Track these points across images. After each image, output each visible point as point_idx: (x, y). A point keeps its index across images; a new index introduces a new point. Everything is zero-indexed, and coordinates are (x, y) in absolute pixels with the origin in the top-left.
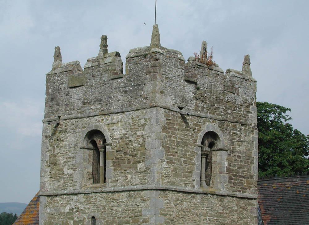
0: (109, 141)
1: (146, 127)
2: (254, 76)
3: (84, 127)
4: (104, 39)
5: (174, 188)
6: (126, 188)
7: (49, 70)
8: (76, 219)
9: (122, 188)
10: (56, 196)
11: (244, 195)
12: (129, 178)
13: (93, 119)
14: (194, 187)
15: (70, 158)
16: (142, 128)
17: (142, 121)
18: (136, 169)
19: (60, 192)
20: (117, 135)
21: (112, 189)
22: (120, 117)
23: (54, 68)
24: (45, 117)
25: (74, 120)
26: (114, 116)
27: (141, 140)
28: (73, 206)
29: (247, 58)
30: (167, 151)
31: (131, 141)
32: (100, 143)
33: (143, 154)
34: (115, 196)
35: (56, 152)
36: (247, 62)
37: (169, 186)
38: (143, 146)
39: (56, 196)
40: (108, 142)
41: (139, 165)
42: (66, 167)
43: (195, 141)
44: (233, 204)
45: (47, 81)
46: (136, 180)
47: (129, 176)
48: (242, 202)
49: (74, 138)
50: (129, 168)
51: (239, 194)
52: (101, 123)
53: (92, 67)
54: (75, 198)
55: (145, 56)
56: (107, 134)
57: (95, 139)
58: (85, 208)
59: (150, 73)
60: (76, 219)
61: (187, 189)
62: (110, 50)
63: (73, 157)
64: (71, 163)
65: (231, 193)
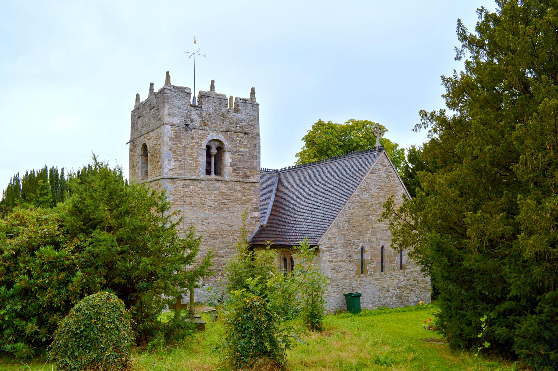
2: (258, 101)
5: (181, 177)
29: (253, 89)
36: (253, 92)
37: (176, 176)
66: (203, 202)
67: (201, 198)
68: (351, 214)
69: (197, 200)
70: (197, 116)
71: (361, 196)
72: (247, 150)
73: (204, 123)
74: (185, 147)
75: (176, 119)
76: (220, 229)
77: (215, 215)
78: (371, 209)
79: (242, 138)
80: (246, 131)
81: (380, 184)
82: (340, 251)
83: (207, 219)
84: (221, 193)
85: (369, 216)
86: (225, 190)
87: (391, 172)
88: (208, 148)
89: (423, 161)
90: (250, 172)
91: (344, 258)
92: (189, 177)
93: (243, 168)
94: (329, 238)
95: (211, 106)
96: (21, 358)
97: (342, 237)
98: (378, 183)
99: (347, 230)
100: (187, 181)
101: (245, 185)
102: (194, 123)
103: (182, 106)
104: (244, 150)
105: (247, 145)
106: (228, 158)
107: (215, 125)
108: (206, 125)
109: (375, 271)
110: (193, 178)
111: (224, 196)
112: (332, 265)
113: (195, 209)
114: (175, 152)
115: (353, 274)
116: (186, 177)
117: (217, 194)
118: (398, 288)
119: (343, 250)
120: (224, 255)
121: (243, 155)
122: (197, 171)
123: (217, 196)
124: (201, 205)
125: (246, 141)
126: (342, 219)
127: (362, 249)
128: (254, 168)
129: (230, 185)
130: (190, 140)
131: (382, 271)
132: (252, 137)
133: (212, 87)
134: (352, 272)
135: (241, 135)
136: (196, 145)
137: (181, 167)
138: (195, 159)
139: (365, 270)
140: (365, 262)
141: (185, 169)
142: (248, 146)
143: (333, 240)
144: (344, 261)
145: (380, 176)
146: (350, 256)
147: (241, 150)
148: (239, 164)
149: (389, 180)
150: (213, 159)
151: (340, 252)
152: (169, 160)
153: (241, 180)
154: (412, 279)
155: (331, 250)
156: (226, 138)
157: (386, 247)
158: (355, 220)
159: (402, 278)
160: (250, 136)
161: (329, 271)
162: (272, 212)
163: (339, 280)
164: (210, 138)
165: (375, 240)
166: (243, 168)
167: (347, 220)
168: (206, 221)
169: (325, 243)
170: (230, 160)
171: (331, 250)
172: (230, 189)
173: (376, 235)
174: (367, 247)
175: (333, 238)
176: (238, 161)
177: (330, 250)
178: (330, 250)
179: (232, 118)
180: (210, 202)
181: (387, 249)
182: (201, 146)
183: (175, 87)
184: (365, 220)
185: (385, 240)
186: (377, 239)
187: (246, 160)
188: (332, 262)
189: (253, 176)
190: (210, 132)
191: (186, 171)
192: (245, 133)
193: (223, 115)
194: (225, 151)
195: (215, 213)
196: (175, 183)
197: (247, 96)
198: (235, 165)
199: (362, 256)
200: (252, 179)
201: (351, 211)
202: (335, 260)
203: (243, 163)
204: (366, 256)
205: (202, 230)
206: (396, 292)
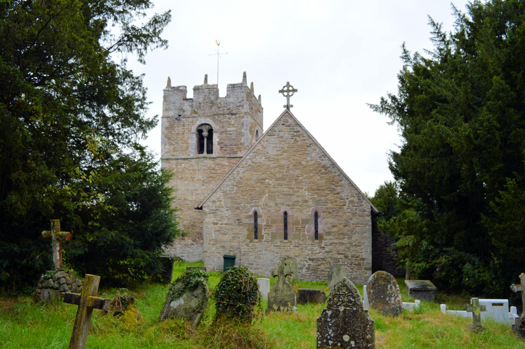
5: (174, 157)
29: (245, 74)
37: (171, 157)
66: (193, 176)
67: (191, 174)
68: (241, 178)
69: (187, 175)
70: (189, 107)
71: (253, 160)
72: (235, 129)
73: (195, 111)
74: (178, 134)
75: (171, 112)
77: (204, 187)
78: (268, 173)
79: (229, 119)
80: (234, 112)
81: (281, 146)
82: (227, 214)
83: (196, 190)
84: (209, 169)
85: (265, 179)
86: (213, 166)
87: (299, 132)
88: (200, 132)
90: (237, 148)
91: (231, 221)
92: (180, 157)
93: (230, 145)
94: (214, 202)
95: (201, 96)
97: (229, 200)
98: (278, 146)
99: (235, 193)
100: (180, 160)
101: (233, 161)
102: (185, 113)
103: (177, 101)
104: (232, 129)
105: (235, 124)
106: (216, 138)
107: (204, 112)
108: (196, 113)
109: (274, 236)
110: (183, 157)
111: (212, 171)
112: (217, 227)
113: (186, 182)
114: (169, 139)
115: (242, 238)
116: (178, 157)
117: (205, 170)
118: (312, 260)
119: (230, 213)
121: (231, 134)
122: (188, 152)
123: (206, 171)
124: (191, 179)
125: (233, 121)
126: (229, 183)
127: (256, 213)
128: (241, 144)
129: (217, 161)
130: (182, 127)
131: (286, 238)
132: (239, 117)
134: (241, 236)
135: (228, 116)
136: (187, 131)
137: (175, 150)
138: (186, 142)
139: (259, 235)
140: (259, 227)
141: (177, 151)
142: (236, 125)
143: (218, 204)
144: (231, 224)
145: (281, 137)
146: (238, 220)
147: (229, 129)
148: (226, 142)
149: (296, 140)
150: (205, 140)
151: (227, 215)
153: (228, 156)
154: (334, 252)
155: (216, 213)
156: (214, 121)
157: (290, 213)
158: (246, 184)
159: (317, 249)
160: (238, 115)
161: (213, 232)
163: (225, 242)
164: (198, 123)
165: (273, 205)
166: (230, 145)
167: (235, 183)
168: (195, 192)
169: (208, 206)
170: (218, 140)
171: (216, 213)
172: (217, 165)
173: (275, 200)
174: (260, 212)
175: (218, 201)
176: (225, 140)
177: (214, 212)
178: (214, 212)
179: (220, 103)
180: (199, 176)
181: (293, 216)
182: (191, 131)
183: (174, 87)
184: (259, 184)
185: (289, 205)
186: (276, 204)
187: (233, 137)
188: (217, 224)
189: (241, 151)
190: (199, 118)
191: (178, 153)
192: (232, 114)
193: (212, 102)
195: (203, 185)
196: (169, 163)
198: (222, 143)
199: (256, 221)
200: (239, 154)
201: (241, 175)
202: (221, 222)
203: (230, 141)
204: (259, 221)
205: (191, 199)
206: (306, 264)
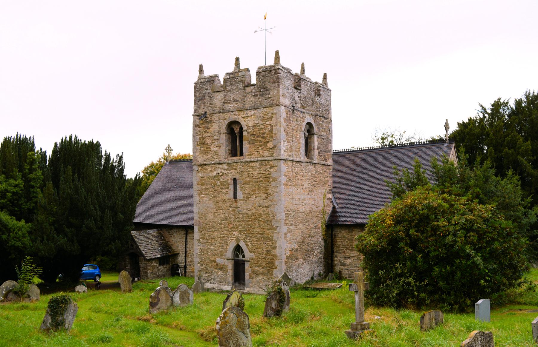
0: (245, 128)
1: (273, 119)
2: (330, 87)
3: (225, 119)
4: (237, 59)
5: (291, 158)
6: (259, 159)
7: (196, 80)
8: (221, 180)
9: (256, 159)
10: (206, 165)
11: (326, 163)
12: (261, 153)
13: (232, 113)
14: (301, 158)
15: (215, 140)
16: (270, 119)
17: (270, 115)
18: (266, 146)
19: (209, 163)
20: (251, 124)
21: (249, 160)
22: (252, 112)
23: (199, 79)
24: (194, 112)
25: (217, 115)
26: (248, 112)
27: (269, 127)
28: (219, 172)
29: (325, 75)
30: (287, 134)
31: (262, 128)
32: (237, 130)
33: (272, 137)
34: (252, 164)
35: (204, 136)
36: (325, 77)
37: (288, 158)
38: (271, 131)
39: (206, 165)
40: (244, 129)
41: (268, 144)
42: (213, 146)
43: (301, 128)
44: (320, 168)
45: (195, 87)
46: (266, 153)
47: (261, 151)
48: (325, 168)
49: (219, 126)
50: (260, 146)
51: (323, 163)
52: (239, 117)
53: (230, 78)
54: (220, 166)
55: (270, 71)
56: (243, 123)
57: (233, 127)
58: (228, 173)
59: (275, 82)
60: (221, 180)
61: (298, 159)
62: (242, 67)
63: (218, 139)
64: (216, 143)
65: (319, 162)
76: (312, 210)
79: (323, 121)
89: (522, 136)
96: (124, 291)
100: (294, 163)
120: (314, 235)
133: (303, 70)
152: (284, 142)
162: (192, 197)
194: (314, 134)
197: (320, 81)
